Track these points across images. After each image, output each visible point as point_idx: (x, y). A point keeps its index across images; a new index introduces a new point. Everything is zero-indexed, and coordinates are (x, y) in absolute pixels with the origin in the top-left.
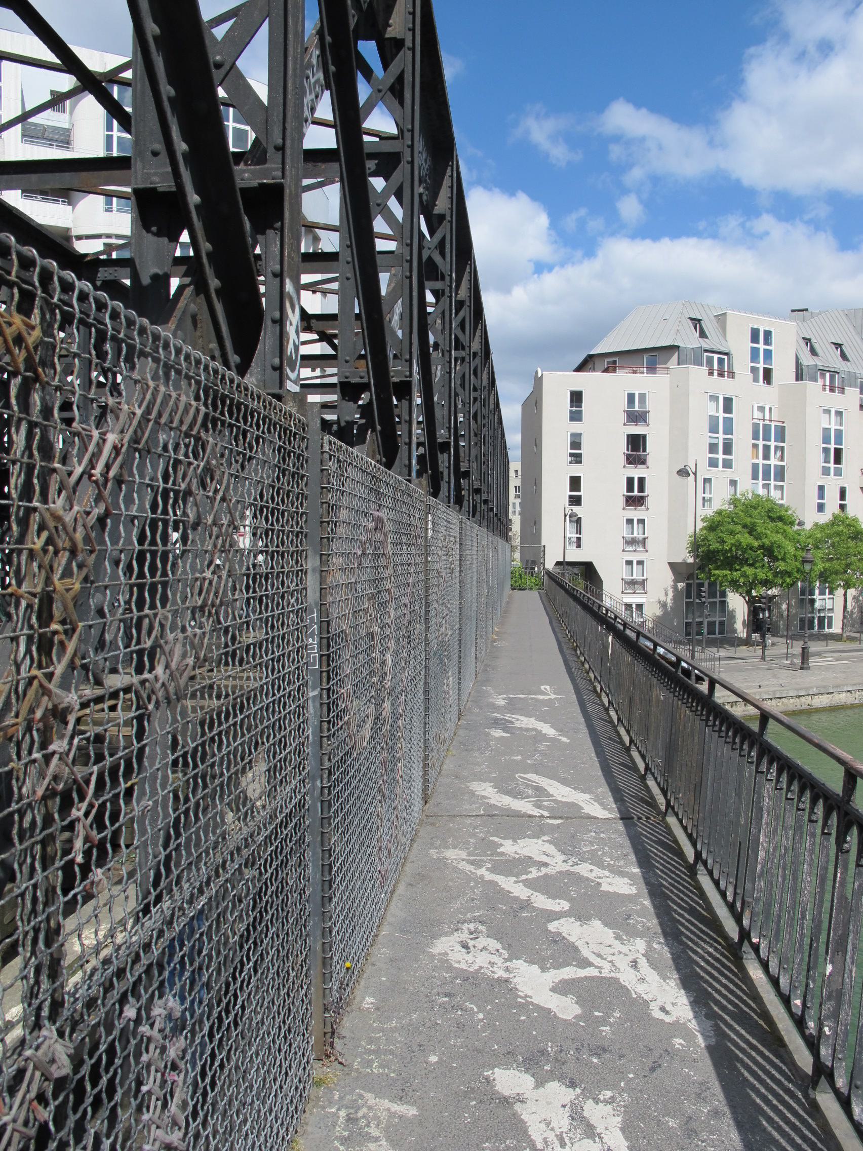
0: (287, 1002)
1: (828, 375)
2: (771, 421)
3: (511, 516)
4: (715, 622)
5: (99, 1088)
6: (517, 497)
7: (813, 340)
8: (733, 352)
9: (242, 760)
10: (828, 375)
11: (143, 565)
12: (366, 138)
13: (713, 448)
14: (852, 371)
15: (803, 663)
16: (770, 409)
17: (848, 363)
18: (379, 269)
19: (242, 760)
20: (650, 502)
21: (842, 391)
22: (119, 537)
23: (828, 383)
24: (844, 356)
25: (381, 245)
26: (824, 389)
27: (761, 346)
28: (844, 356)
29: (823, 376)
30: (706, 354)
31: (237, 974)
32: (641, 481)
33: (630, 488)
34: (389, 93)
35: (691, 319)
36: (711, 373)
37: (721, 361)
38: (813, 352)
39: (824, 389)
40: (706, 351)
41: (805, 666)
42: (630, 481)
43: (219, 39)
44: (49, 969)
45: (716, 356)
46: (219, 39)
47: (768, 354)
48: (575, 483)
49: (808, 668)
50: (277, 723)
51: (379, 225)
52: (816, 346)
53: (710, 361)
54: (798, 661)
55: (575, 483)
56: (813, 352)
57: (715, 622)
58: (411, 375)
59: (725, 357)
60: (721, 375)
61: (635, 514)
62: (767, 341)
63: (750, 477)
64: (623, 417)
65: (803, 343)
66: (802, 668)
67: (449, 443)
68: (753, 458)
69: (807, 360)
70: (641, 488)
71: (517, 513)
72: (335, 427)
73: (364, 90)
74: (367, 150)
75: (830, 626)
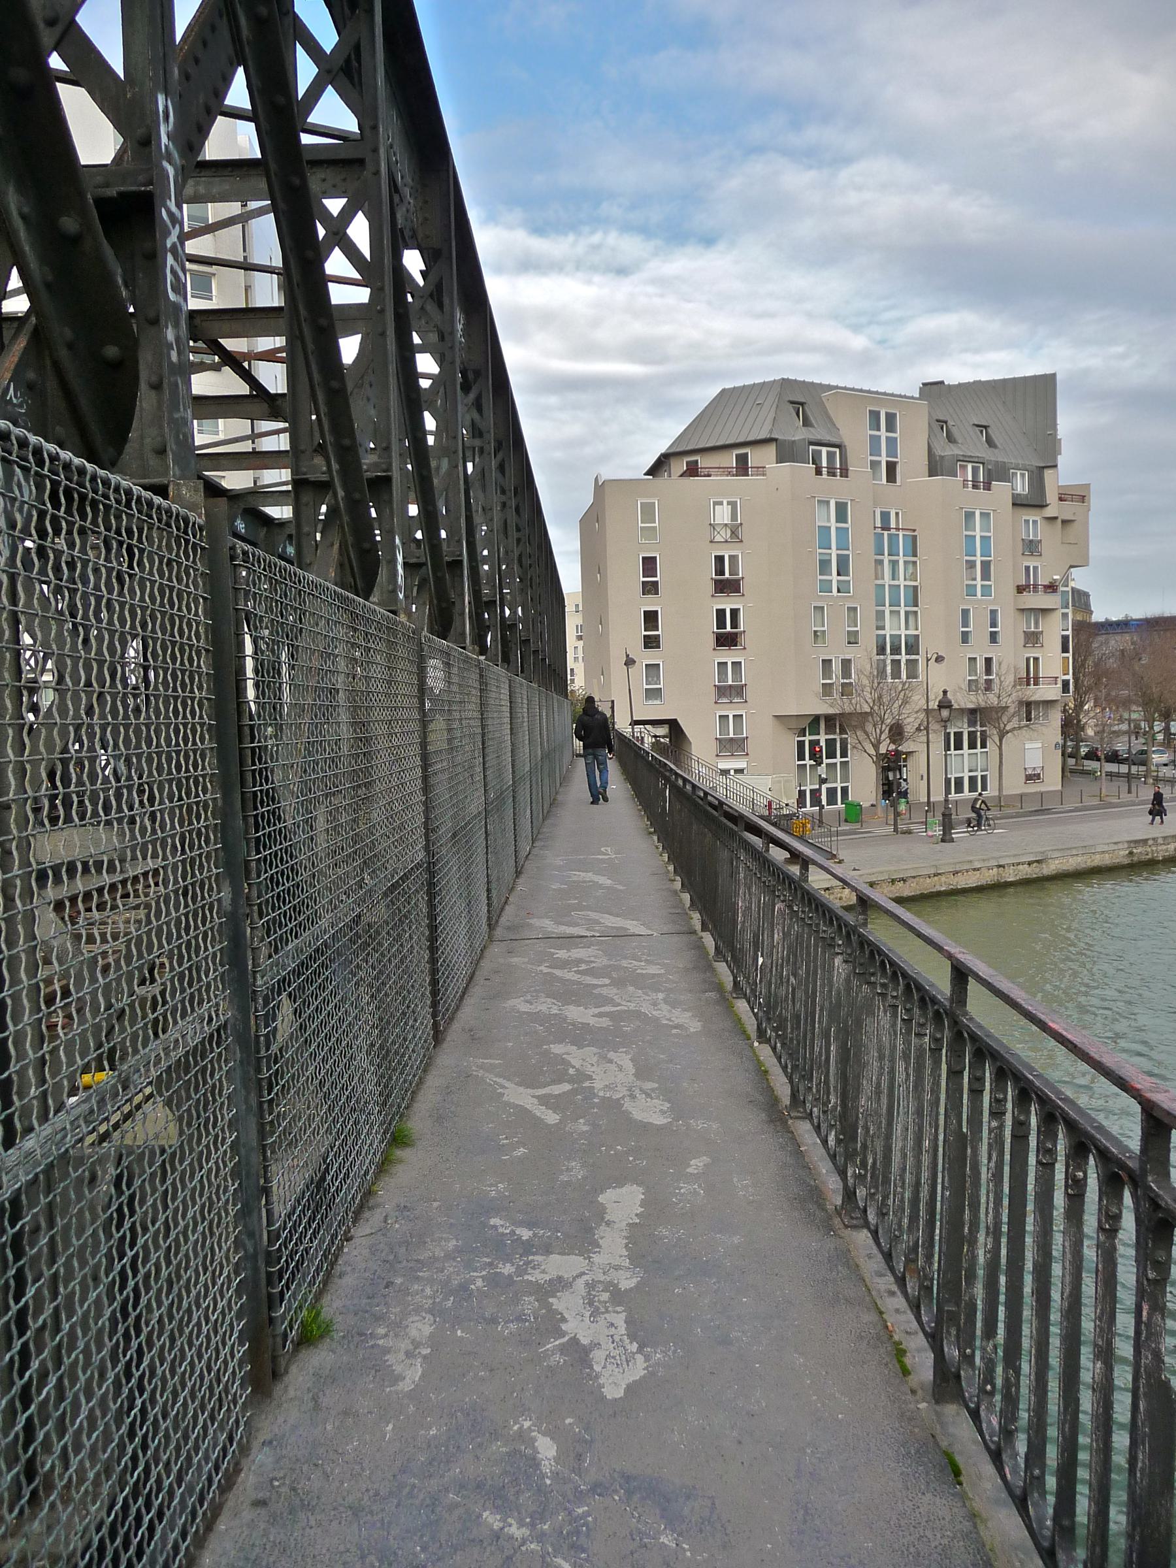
1: (970, 466)
2: (898, 529)
3: (570, 664)
4: (836, 788)
5: (25, 1415)
6: (580, 638)
7: (950, 423)
8: (847, 442)
9: (190, 986)
10: (970, 466)
12: (306, 139)
13: (824, 565)
14: (1000, 459)
15: (944, 834)
16: (897, 514)
17: (996, 451)
18: (338, 325)
19: (190, 986)
20: (747, 640)
21: (988, 487)
22: (67, 710)
24: (990, 442)
25: (340, 295)
27: (883, 433)
28: (990, 442)
29: (964, 468)
30: (811, 447)
31: (182, 1272)
32: (735, 613)
33: (721, 623)
35: (792, 402)
36: (818, 472)
37: (831, 456)
38: (950, 438)
41: (947, 838)
42: (721, 613)
43: (335, 214)
45: (824, 450)
46: (335, 214)
47: (891, 442)
48: (651, 618)
49: (952, 840)
50: (193, 942)
51: (337, 263)
52: (954, 431)
53: (816, 460)
54: (938, 831)
55: (651, 618)
56: (950, 438)
57: (836, 788)
58: (389, 469)
59: (837, 450)
60: (832, 473)
61: (729, 656)
62: (891, 427)
63: (874, 603)
64: (711, 641)
65: (936, 426)
66: (943, 841)
67: (461, 562)
68: (877, 578)
69: (945, 450)
70: (735, 624)
71: (580, 659)
72: (444, 605)
74: (307, 156)
75: (984, 788)
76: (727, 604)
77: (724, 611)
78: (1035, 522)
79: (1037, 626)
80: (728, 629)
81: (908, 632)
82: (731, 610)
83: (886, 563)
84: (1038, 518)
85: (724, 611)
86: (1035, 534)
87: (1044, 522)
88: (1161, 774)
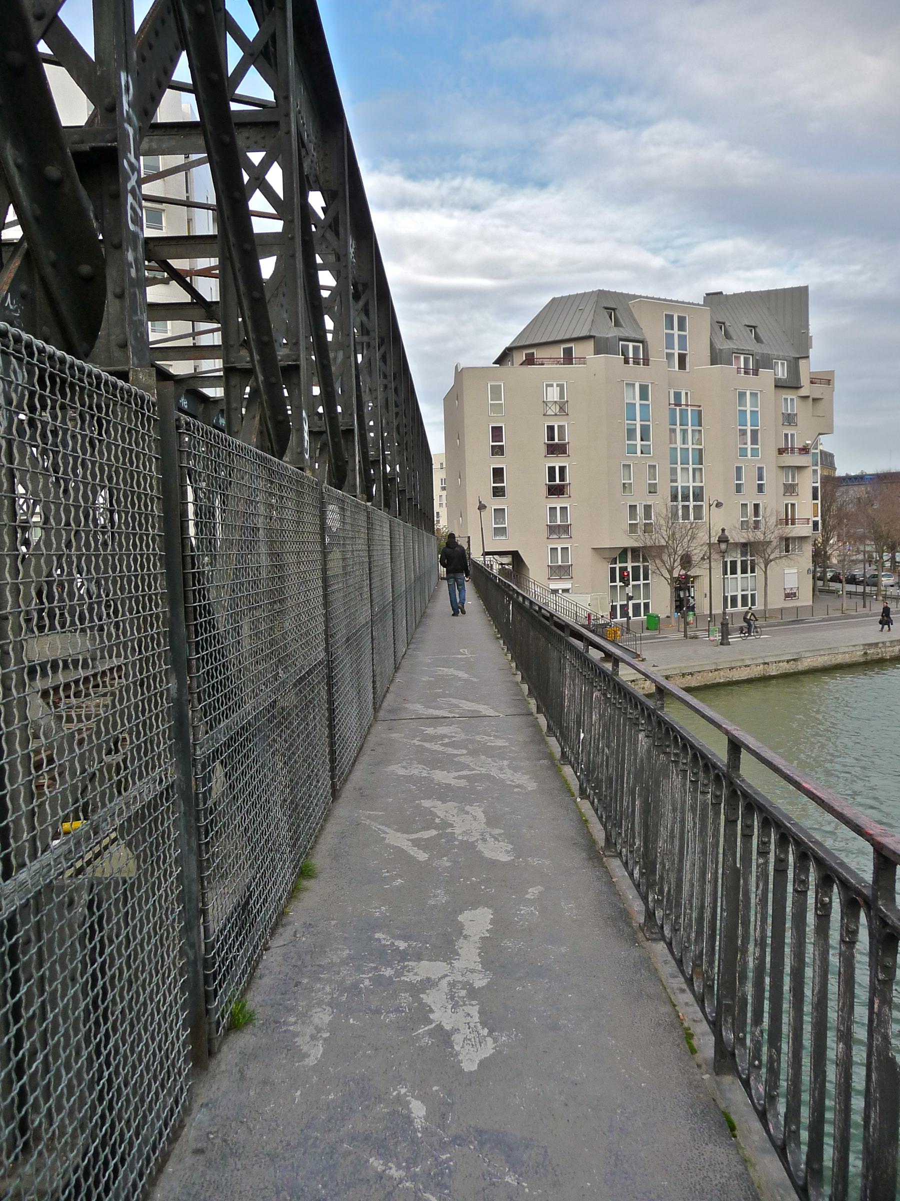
0: (163, 1028)
1: (742, 357)
2: (687, 405)
3: (436, 508)
4: (640, 604)
7: (727, 324)
10: (742, 357)
11: (36, 564)
12: (234, 106)
13: (631, 433)
14: (765, 352)
15: (722, 639)
16: (687, 394)
17: (762, 345)
18: (259, 249)
20: (571, 490)
21: (756, 373)
22: (52, 544)
23: (742, 366)
24: (758, 339)
26: (738, 372)
27: (676, 332)
28: (758, 339)
29: (738, 358)
30: (621, 343)
32: (562, 469)
33: (552, 477)
34: (261, 56)
36: (626, 361)
37: (636, 349)
38: (727, 336)
39: (738, 372)
40: (621, 340)
41: (725, 641)
42: (552, 470)
44: (434, 768)
45: (631, 345)
46: (257, 164)
48: (498, 474)
49: (729, 644)
51: (258, 202)
52: (730, 330)
53: (624, 353)
54: (718, 637)
55: (498, 474)
56: (727, 336)
57: (640, 604)
58: (298, 359)
59: (641, 345)
60: (636, 362)
61: (558, 503)
62: (682, 327)
64: (544, 491)
65: (717, 327)
66: (722, 644)
67: (353, 430)
68: (671, 443)
69: (723, 345)
70: (562, 478)
71: (444, 505)
73: (234, 54)
74: (235, 120)
75: (753, 604)
76: (557, 462)
77: (554, 468)
78: (792, 400)
79: (793, 479)
80: (558, 481)
81: (695, 484)
82: (560, 467)
83: (678, 431)
84: (794, 397)
85: (554, 468)
86: (792, 409)
87: (799, 400)
88: (888, 593)
